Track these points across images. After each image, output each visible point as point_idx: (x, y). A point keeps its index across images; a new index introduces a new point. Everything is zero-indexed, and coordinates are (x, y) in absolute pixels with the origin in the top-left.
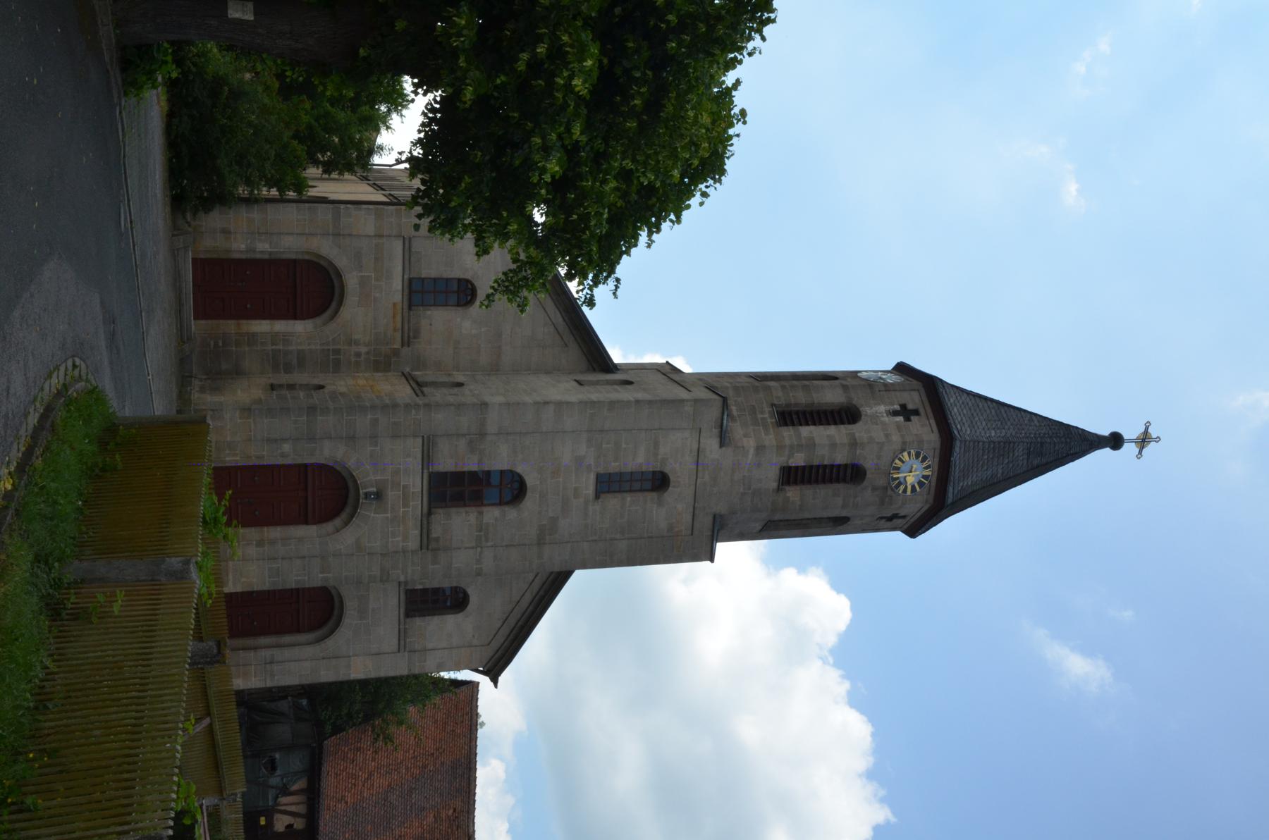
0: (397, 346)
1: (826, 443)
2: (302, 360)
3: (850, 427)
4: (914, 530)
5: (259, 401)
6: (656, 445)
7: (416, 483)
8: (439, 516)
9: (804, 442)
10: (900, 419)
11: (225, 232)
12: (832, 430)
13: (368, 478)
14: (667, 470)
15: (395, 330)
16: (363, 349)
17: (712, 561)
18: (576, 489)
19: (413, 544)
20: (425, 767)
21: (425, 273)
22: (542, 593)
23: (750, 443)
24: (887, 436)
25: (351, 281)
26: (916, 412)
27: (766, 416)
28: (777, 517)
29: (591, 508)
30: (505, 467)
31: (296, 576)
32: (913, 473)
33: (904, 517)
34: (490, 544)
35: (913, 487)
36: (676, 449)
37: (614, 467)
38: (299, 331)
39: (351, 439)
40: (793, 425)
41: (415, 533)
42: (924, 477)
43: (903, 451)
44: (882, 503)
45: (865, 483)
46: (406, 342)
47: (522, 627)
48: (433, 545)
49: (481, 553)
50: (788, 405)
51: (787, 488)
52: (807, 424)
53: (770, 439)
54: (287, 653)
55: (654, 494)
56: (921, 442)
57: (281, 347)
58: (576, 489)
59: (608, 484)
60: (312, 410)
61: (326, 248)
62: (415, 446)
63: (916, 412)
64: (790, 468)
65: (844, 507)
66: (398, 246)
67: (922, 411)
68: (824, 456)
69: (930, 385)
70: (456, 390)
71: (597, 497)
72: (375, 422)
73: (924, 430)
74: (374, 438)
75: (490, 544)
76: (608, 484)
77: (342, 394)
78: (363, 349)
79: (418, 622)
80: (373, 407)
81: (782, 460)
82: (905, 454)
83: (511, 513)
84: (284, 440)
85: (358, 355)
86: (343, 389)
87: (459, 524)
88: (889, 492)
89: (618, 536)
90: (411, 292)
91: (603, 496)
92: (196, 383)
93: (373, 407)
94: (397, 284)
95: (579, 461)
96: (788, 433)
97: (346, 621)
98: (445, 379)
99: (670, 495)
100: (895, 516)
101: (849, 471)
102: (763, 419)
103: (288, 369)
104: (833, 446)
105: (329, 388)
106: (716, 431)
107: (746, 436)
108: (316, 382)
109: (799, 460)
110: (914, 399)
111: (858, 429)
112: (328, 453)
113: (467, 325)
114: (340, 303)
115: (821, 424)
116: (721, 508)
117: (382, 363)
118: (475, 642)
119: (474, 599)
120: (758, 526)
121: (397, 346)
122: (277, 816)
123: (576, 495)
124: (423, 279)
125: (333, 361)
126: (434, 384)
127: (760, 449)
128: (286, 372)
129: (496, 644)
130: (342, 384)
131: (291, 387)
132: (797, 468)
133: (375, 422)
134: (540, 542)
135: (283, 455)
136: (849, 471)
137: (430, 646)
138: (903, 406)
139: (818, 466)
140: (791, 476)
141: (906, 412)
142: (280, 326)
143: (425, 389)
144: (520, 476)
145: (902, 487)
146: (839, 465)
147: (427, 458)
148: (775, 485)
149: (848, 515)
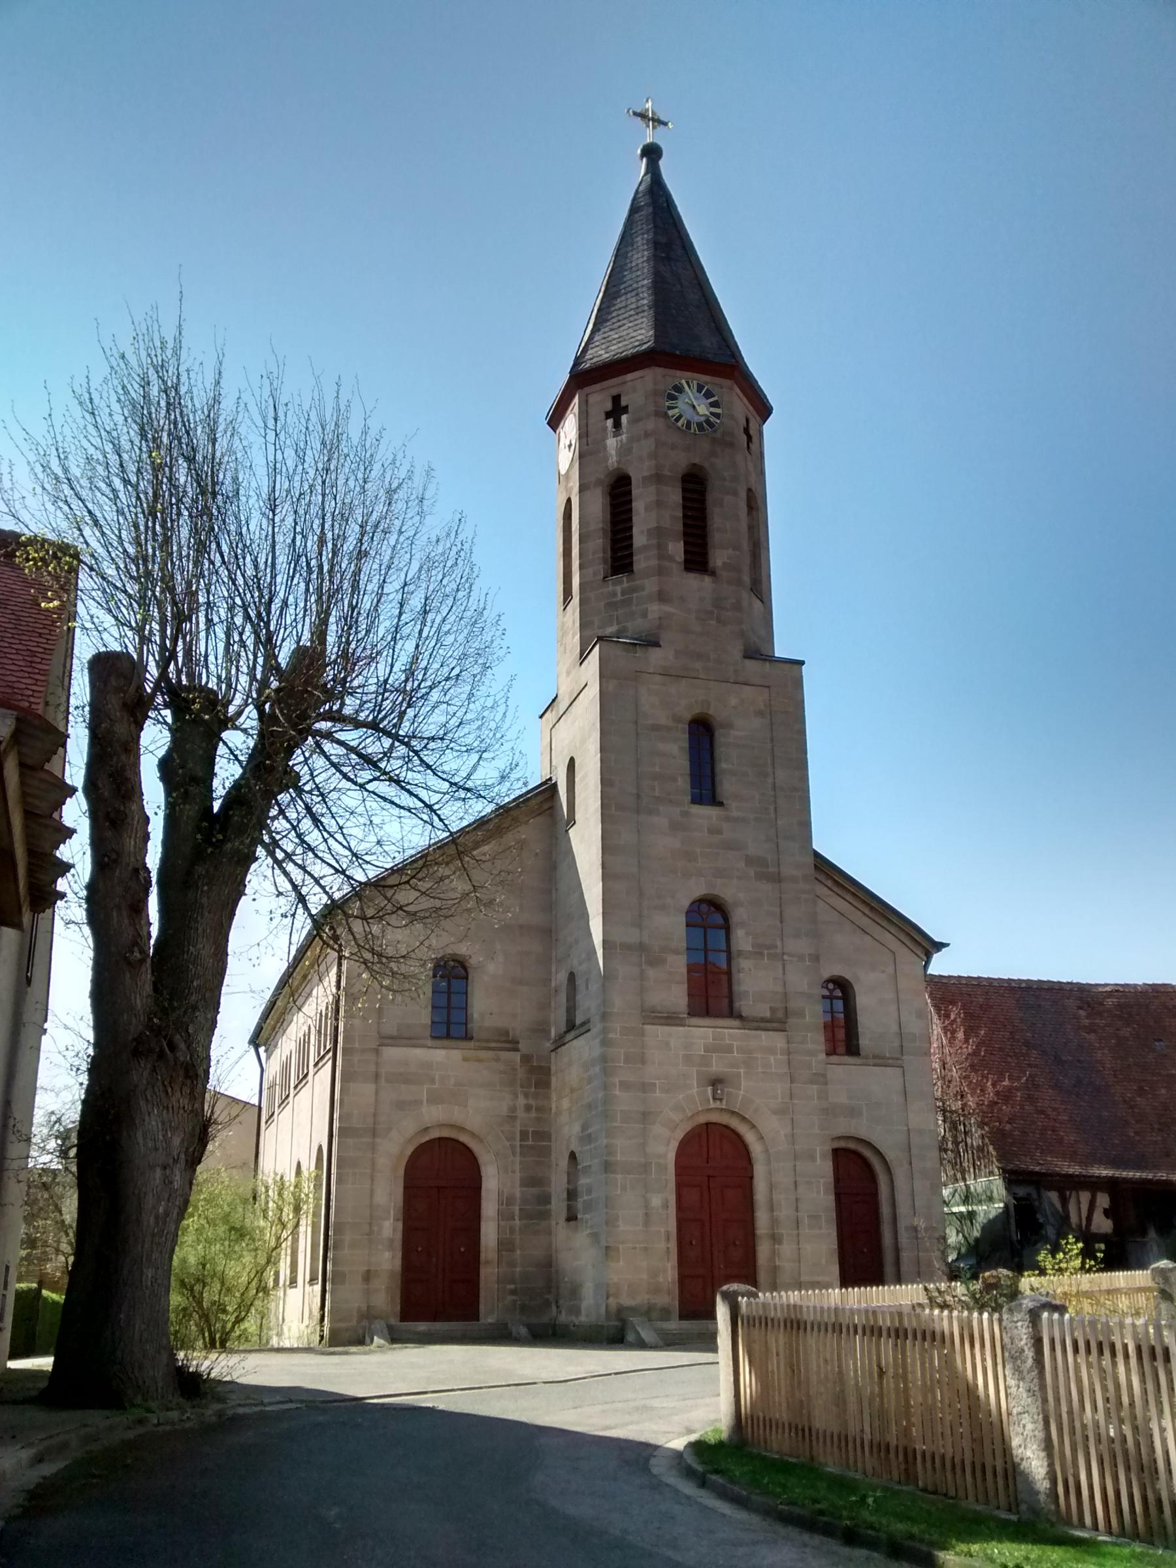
0: (516, 1057)
2: (535, 1181)
3: (633, 482)
4: (764, 410)
5: (595, 1237)
6: (656, 728)
8: (746, 1006)
9: (654, 541)
10: (624, 419)
11: (368, 1277)
14: (688, 716)
15: (497, 1060)
16: (521, 1101)
17: (802, 663)
19: (776, 1040)
20: (1027, 1043)
21: (428, 1021)
22: (829, 883)
24: (647, 435)
26: (616, 399)
27: (619, 589)
28: (746, 579)
29: (735, 814)
30: (682, 919)
31: (819, 1196)
32: (694, 404)
33: (747, 421)
34: (779, 943)
35: (713, 405)
36: (666, 705)
37: (683, 783)
38: (496, 1182)
39: (645, 1117)
40: (631, 555)
41: (766, 1038)
42: (699, 391)
43: (666, 415)
44: (731, 445)
45: (706, 465)
46: (512, 1044)
47: (872, 909)
48: (780, 1015)
49: (789, 955)
50: (605, 561)
51: (711, 565)
52: (631, 537)
53: (650, 585)
54: (903, 1209)
55: (718, 734)
56: (655, 393)
57: (517, 1208)
59: (705, 788)
60: (608, 1167)
62: (657, 1032)
63: (616, 399)
64: (686, 561)
66: (392, 1053)
67: (615, 392)
68: (673, 515)
69: (582, 378)
70: (580, 982)
71: (721, 804)
72: (625, 1086)
73: (638, 388)
74: (645, 1087)
75: (779, 943)
76: (705, 788)
77: (584, 1127)
78: (521, 1101)
80: (605, 1087)
82: (670, 413)
83: (738, 915)
84: (647, 1206)
85: (528, 1108)
86: (576, 1128)
87: (754, 983)
88: (718, 435)
89: (770, 780)
90: (448, 1036)
91: (719, 799)
92: (563, 1318)
93: (605, 1087)
96: (641, 562)
97: (863, 1133)
98: (563, 998)
99: (718, 713)
100: (746, 431)
101: (691, 486)
102: (623, 594)
103: (545, 1199)
104: (659, 504)
105: (575, 1146)
106: (640, 653)
107: (644, 614)
108: (564, 1163)
109: (677, 549)
111: (638, 473)
112: (664, 1149)
113: (491, 968)
114: (462, 1129)
115: (631, 519)
117: (538, 1077)
118: (890, 970)
119: (837, 970)
120: (757, 604)
121: (516, 1057)
122: (1094, 1228)
123: (719, 832)
124: (433, 1022)
125: (535, 1142)
126: (571, 1009)
128: (550, 1203)
129: (893, 943)
130: (568, 1131)
131: (572, 1195)
132: (686, 552)
133: (625, 1086)
134: (777, 879)
135: (666, 1206)
136: (691, 486)
137: (894, 1028)
138: (608, 415)
139: (685, 525)
140: (697, 559)
141: (616, 411)
142: (489, 1208)
143: (578, 1022)
144: (693, 903)
145: (712, 419)
146: (684, 498)
147: (671, 1019)
148: (707, 579)
149: (745, 488)
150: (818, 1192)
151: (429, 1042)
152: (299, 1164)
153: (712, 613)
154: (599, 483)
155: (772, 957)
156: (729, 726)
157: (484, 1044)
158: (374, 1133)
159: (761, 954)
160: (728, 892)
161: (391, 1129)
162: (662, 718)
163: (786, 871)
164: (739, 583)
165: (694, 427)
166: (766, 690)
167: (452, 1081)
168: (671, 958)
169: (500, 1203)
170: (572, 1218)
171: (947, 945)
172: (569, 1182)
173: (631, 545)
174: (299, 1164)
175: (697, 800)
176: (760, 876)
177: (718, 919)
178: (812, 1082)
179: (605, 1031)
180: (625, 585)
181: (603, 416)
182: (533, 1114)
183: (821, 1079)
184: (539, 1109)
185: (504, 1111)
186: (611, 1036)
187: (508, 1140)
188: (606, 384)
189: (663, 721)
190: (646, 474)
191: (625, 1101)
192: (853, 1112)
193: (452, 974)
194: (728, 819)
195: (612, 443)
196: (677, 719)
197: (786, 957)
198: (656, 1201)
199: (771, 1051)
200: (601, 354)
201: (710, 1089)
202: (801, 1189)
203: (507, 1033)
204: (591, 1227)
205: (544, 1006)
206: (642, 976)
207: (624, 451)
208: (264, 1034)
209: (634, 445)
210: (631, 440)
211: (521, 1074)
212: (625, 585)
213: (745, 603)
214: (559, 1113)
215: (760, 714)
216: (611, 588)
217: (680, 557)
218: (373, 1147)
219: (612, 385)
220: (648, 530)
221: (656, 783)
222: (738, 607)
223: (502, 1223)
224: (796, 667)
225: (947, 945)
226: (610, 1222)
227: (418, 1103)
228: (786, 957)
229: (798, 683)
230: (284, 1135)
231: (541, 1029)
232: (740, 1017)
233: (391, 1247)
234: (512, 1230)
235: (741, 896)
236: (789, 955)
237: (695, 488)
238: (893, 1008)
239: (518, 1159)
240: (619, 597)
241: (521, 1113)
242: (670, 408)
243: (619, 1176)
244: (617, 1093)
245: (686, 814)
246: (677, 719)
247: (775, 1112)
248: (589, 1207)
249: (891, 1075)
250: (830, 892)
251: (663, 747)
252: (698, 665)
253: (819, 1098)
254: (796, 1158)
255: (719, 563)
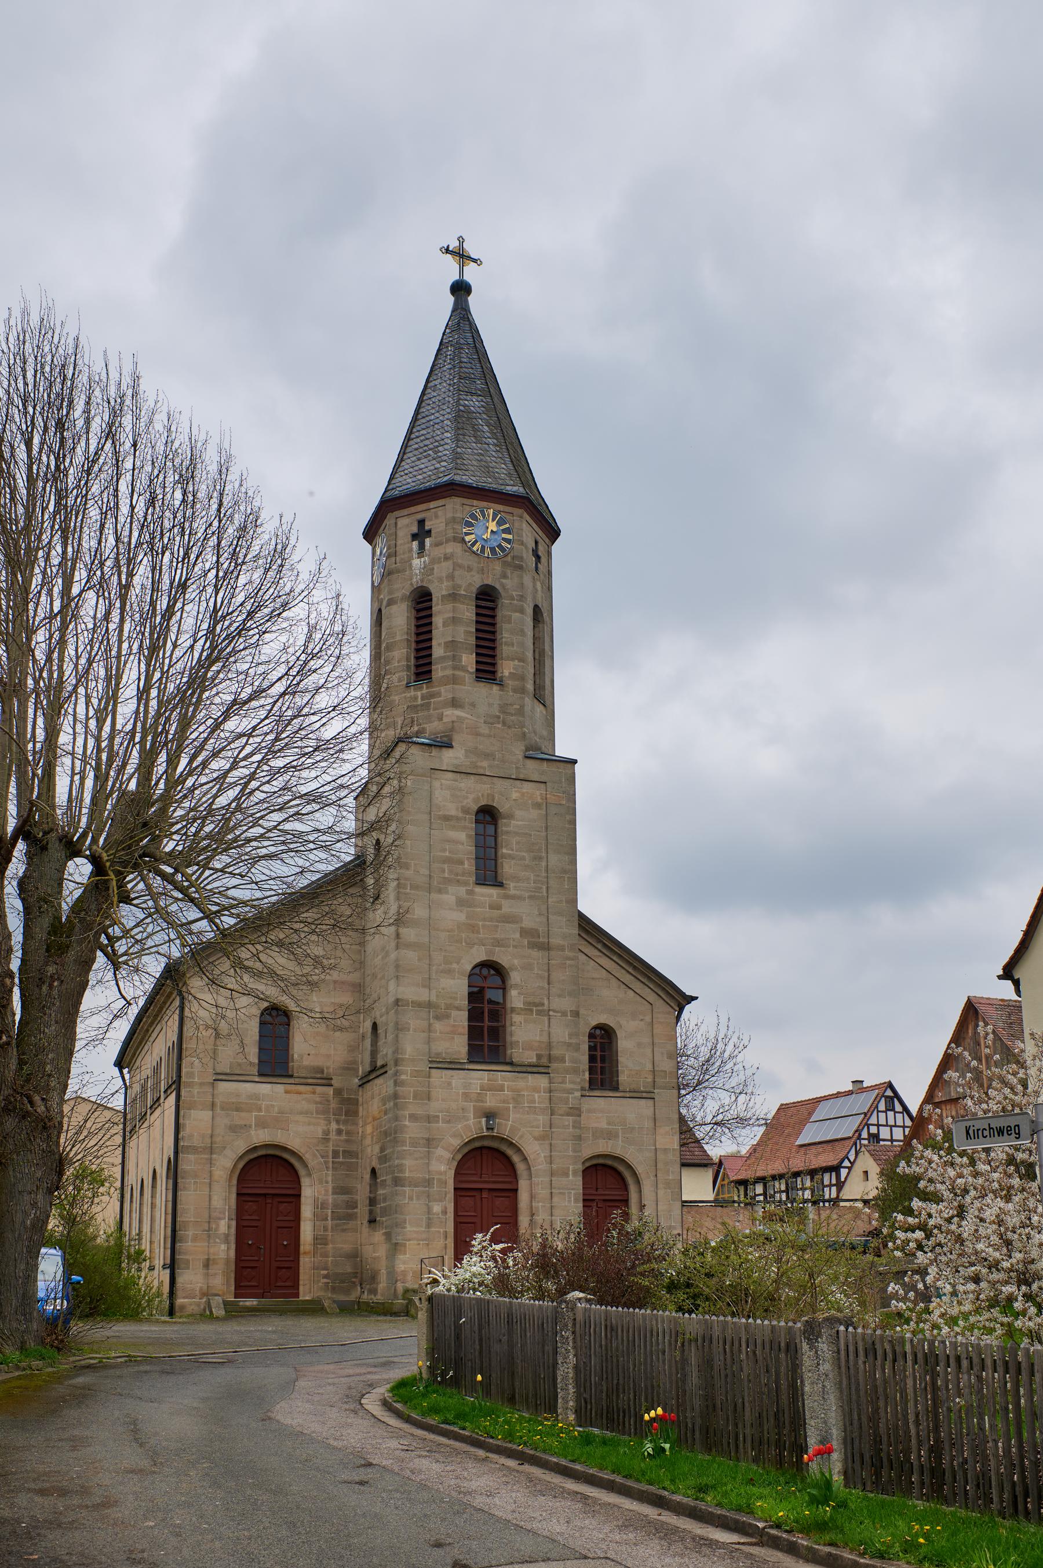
0: (330, 1091)
1: (453, 628)
3: (434, 599)
4: (553, 533)
6: (447, 818)
7: (478, 1078)
10: (428, 541)
12: (438, 621)
13: (471, 1127)
14: (475, 808)
15: (314, 1093)
17: (575, 762)
18: (491, 907)
19: (542, 1081)
23: (451, 714)
25: (261, 1137)
26: (421, 523)
27: (419, 694)
28: (530, 686)
29: (512, 892)
33: (536, 543)
34: (546, 1002)
39: (429, 1142)
44: (520, 567)
47: (635, 968)
48: (544, 1061)
52: (430, 647)
53: (445, 692)
55: (502, 822)
58: (491, 907)
59: (488, 871)
60: (397, 1182)
61: (226, 1163)
62: (439, 1077)
63: (421, 523)
65: (522, 611)
66: (223, 1087)
67: (420, 516)
68: (465, 632)
70: (380, 1031)
71: (501, 885)
72: (413, 1117)
73: (441, 515)
75: (546, 1002)
76: (488, 871)
77: (382, 1149)
78: (334, 1126)
79: (623, 1078)
81: (469, 678)
82: (467, 538)
83: (515, 978)
84: (429, 1211)
85: (339, 1132)
87: (524, 1034)
89: (544, 864)
91: (499, 879)
94: (265, 1089)
95: (461, 903)
96: (439, 671)
97: (618, 1152)
102: (423, 698)
103: (353, 1205)
105: (375, 1163)
106: (435, 752)
107: (440, 718)
109: (469, 660)
110: (404, 523)
111: (438, 591)
114: (285, 1149)
116: (518, 750)
118: (648, 1018)
120: (539, 709)
126: (374, 1053)
127: (455, 703)
129: (651, 997)
131: (372, 1202)
133: (413, 1117)
134: (546, 947)
135: (445, 1212)
137: (649, 1067)
138: (414, 537)
140: (487, 670)
141: (421, 534)
142: (307, 1211)
148: (495, 688)
150: (570, 1201)
151: (257, 1079)
152: (155, 1171)
153: (499, 717)
154: (403, 598)
155: (539, 1013)
156: (511, 816)
157: (303, 1081)
158: (211, 1150)
159: (532, 1010)
160: (503, 958)
161: (225, 1148)
162: (452, 810)
163: (555, 941)
164: (523, 690)
165: (487, 551)
166: (543, 785)
167: (276, 1109)
168: (454, 1013)
169: (316, 1206)
170: (372, 1221)
171: (697, 998)
172: (370, 1192)
173: (431, 655)
174: (155, 1171)
175: (481, 881)
176: (533, 945)
177: (498, 981)
178: (568, 1115)
179: (396, 1073)
180: (425, 691)
181: (410, 538)
182: (344, 1137)
183: (576, 1112)
184: (348, 1133)
185: (319, 1132)
186: (403, 1077)
187: (322, 1157)
188: (413, 509)
189: (453, 813)
190: (444, 593)
191: (412, 1130)
192: (611, 1135)
193: (276, 1021)
194: (507, 897)
195: (417, 563)
196: (466, 811)
197: (551, 1013)
198: (437, 1208)
199: (536, 1089)
200: (408, 483)
201: (484, 1120)
202: (555, 1199)
203: (322, 1072)
204: (386, 1228)
205: (353, 1049)
206: (430, 1029)
207: (428, 570)
208: (127, 1059)
209: (436, 567)
210: (433, 561)
211: (333, 1105)
212: (425, 691)
213: (528, 708)
214: (363, 1137)
215: (538, 806)
216: (413, 693)
217: (472, 668)
218: (211, 1162)
219: (419, 511)
220: (445, 643)
221: (446, 866)
222: (521, 712)
223: (317, 1223)
224: (569, 765)
225: (697, 998)
226: (401, 1225)
227: (247, 1127)
228: (551, 1013)
229: (572, 779)
230: (143, 1146)
231: (349, 1068)
232: (511, 1064)
233: (226, 1241)
234: (326, 1229)
235: (516, 962)
236: (554, 1011)
237: (422, 668)
238: (649, 1051)
239: (330, 1172)
240: (419, 702)
241: (333, 1136)
242: (467, 534)
243: (407, 1189)
244: (407, 1123)
245: (470, 892)
246: (466, 811)
247: (536, 1139)
248: (385, 1212)
249: (644, 1107)
250: (599, 954)
251: (452, 834)
252: (485, 764)
253: (573, 1127)
254: (552, 1175)
255: (506, 673)
